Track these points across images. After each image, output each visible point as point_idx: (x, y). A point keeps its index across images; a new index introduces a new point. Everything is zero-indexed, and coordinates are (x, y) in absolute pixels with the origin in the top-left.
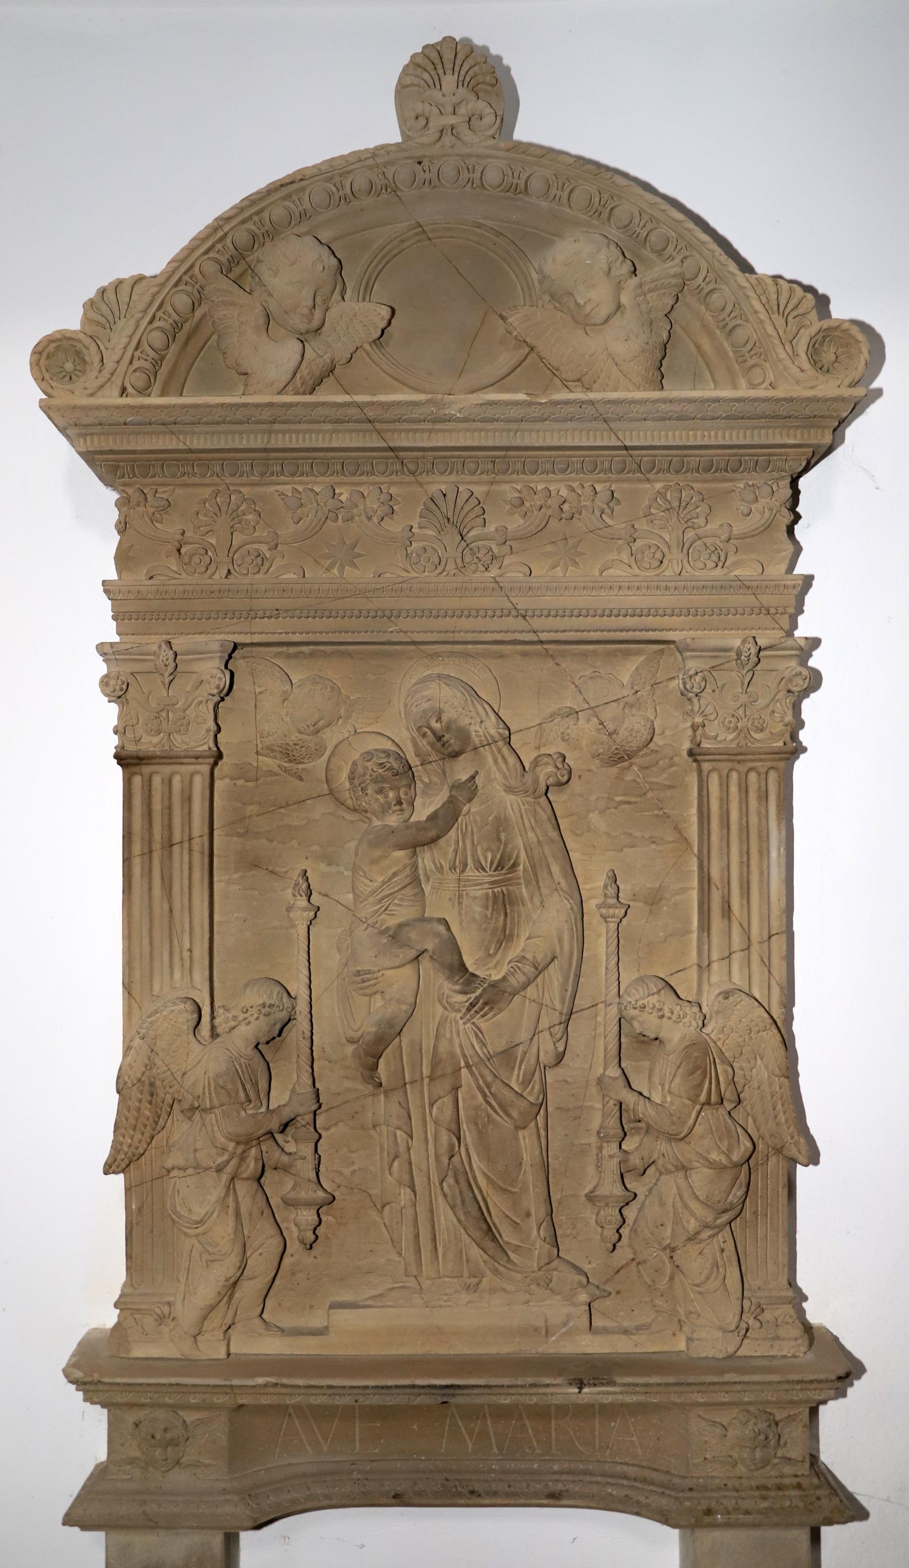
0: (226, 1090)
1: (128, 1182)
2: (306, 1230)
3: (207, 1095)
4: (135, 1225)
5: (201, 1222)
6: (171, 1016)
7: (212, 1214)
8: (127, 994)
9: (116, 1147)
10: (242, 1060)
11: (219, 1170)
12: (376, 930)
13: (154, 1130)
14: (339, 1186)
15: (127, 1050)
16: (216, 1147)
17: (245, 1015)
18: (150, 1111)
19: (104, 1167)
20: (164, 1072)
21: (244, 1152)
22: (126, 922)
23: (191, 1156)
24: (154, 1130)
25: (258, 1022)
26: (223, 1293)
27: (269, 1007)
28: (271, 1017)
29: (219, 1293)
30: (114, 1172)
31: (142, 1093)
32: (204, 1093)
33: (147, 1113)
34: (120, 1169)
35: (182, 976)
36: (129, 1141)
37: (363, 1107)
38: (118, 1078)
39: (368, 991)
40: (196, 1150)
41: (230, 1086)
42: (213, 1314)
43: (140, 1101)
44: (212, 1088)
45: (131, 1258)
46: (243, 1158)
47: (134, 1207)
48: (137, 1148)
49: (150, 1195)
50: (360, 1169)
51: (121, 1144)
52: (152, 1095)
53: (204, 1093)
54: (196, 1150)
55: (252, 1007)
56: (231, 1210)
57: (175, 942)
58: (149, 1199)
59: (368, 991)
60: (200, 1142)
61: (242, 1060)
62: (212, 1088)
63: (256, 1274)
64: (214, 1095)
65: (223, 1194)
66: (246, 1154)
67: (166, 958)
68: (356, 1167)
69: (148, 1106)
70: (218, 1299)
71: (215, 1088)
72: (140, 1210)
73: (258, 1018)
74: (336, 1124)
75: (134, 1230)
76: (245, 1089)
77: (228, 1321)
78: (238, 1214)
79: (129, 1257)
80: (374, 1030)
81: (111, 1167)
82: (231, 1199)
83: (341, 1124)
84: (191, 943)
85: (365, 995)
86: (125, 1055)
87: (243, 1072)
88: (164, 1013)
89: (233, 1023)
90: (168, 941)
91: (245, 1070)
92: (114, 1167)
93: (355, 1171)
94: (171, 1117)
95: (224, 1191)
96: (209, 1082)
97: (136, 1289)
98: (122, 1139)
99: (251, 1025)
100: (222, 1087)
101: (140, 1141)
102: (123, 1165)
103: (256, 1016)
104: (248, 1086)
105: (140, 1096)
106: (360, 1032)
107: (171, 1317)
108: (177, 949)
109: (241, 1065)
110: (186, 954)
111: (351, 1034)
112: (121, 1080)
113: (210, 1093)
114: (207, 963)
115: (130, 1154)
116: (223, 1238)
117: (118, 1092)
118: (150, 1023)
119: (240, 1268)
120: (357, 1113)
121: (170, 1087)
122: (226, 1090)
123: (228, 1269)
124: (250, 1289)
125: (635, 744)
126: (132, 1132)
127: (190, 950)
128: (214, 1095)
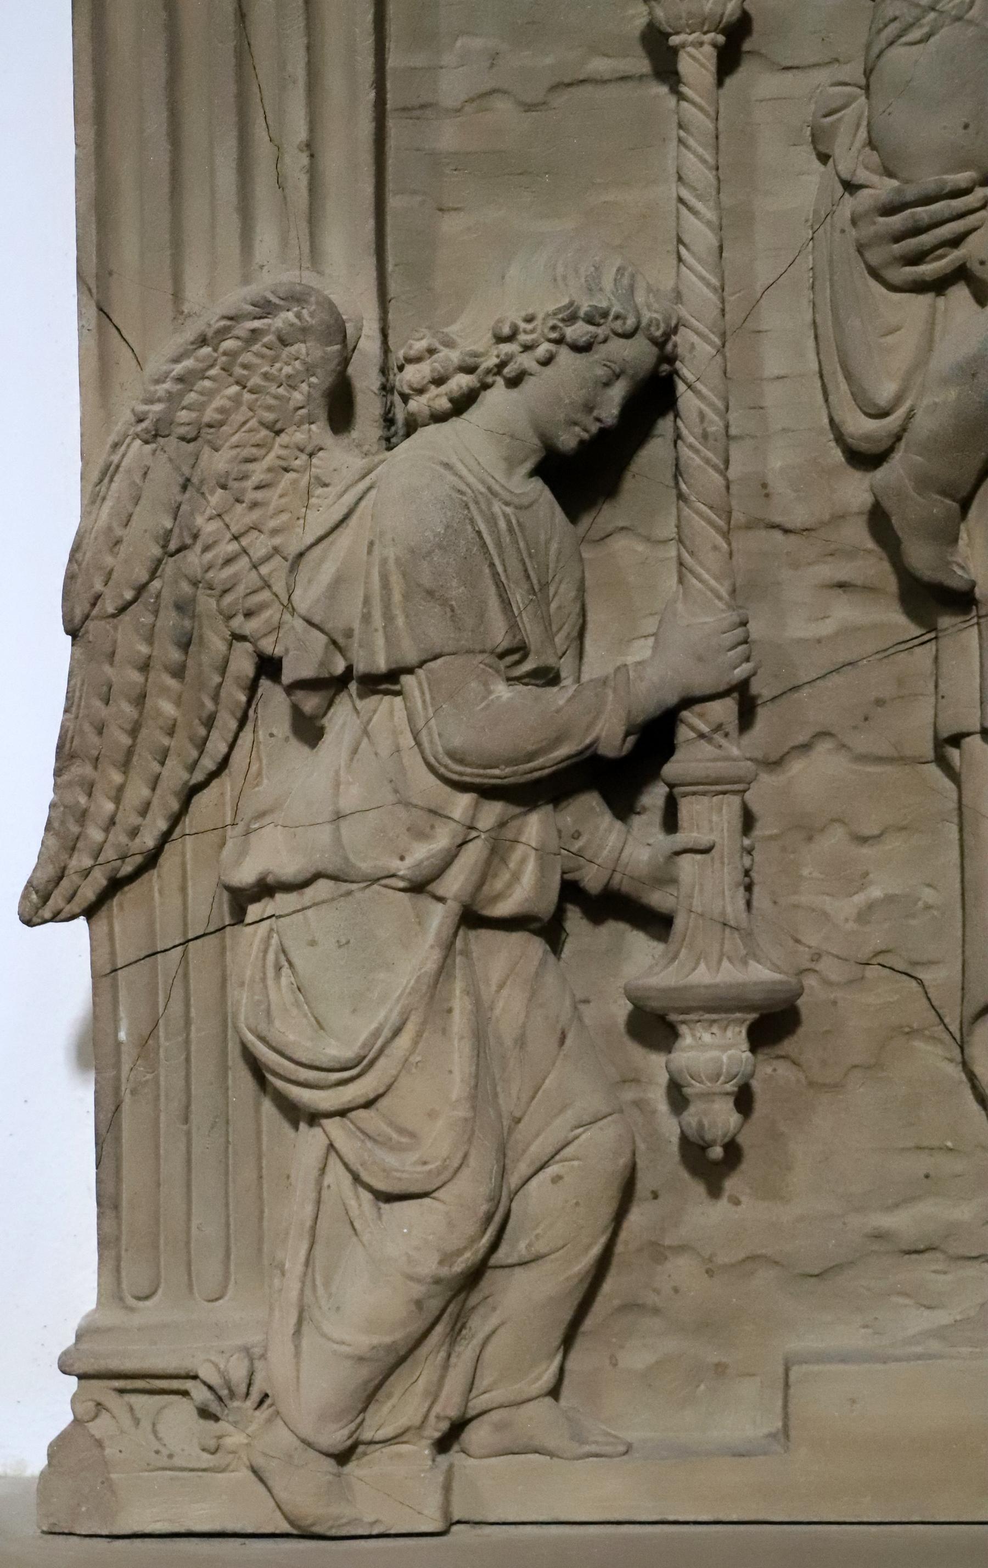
0: (444, 602)
1: (104, 950)
2: (707, 1096)
3: (378, 620)
4: (127, 1098)
5: (359, 1066)
6: (247, 357)
7: (397, 1032)
8: (93, 311)
9: (65, 827)
10: (497, 507)
11: (418, 887)
12: (971, 31)
13: (192, 768)
14: (817, 956)
15: (99, 480)
16: (408, 805)
17: (506, 348)
18: (178, 703)
19: (25, 896)
20: (228, 561)
21: (502, 824)
22: (86, 59)
23: (324, 835)
24: (192, 768)
25: (548, 371)
26: (434, 1305)
27: (590, 321)
28: (601, 352)
29: (419, 1304)
30: (55, 918)
31: (150, 639)
32: (366, 618)
33: (168, 708)
34: (75, 907)
35: (284, 242)
36: (109, 806)
37: (900, 682)
38: (70, 578)
39: (928, 269)
40: (339, 817)
41: (456, 591)
42: (397, 1383)
43: (145, 667)
44: (397, 597)
45: (116, 1207)
46: (498, 850)
47: (122, 1036)
48: (134, 832)
49: (178, 993)
50: (890, 899)
51: (82, 817)
52: (185, 645)
53: (366, 618)
54: (339, 817)
55: (529, 319)
56: (459, 1021)
57: (260, 132)
58: (176, 1007)
59: (928, 269)
60: (355, 790)
61: (497, 507)
62: (397, 597)
63: (541, 1247)
64: (400, 621)
65: (431, 966)
66: (509, 833)
67: (226, 178)
68: (876, 892)
69: (172, 683)
70: (416, 1327)
71: (406, 597)
72: (146, 1042)
73: (547, 362)
74: (805, 747)
75: (126, 1107)
76: (506, 604)
77: (449, 1407)
78: (480, 1036)
79: (108, 1202)
80: (953, 394)
81: (45, 899)
82: (459, 986)
83: (824, 746)
84: (312, 130)
85: (919, 287)
86: (93, 497)
87: (499, 545)
88: (229, 344)
89: (462, 382)
90: (232, 118)
91: (507, 539)
92: (57, 900)
93: (871, 906)
94: (249, 727)
95: (436, 955)
96: (385, 579)
97: (132, 1309)
98: (83, 800)
99: (529, 385)
100: (430, 593)
101: (144, 811)
102: (88, 893)
103: (543, 349)
104: (518, 597)
105: (144, 649)
106: (901, 412)
107: (255, 1396)
108: (263, 149)
109: (492, 520)
110: (296, 163)
111: (860, 426)
112: (78, 585)
113: (389, 618)
114: (369, 189)
115: (109, 853)
116: (432, 1115)
117: (73, 631)
118: (180, 379)
119: (489, 1218)
120: (880, 702)
121: (248, 614)
122: (444, 602)
123: (451, 1225)
124: (523, 1299)
125: (750, 1068)
126: (117, 778)
127: (310, 148)
128: (400, 621)
